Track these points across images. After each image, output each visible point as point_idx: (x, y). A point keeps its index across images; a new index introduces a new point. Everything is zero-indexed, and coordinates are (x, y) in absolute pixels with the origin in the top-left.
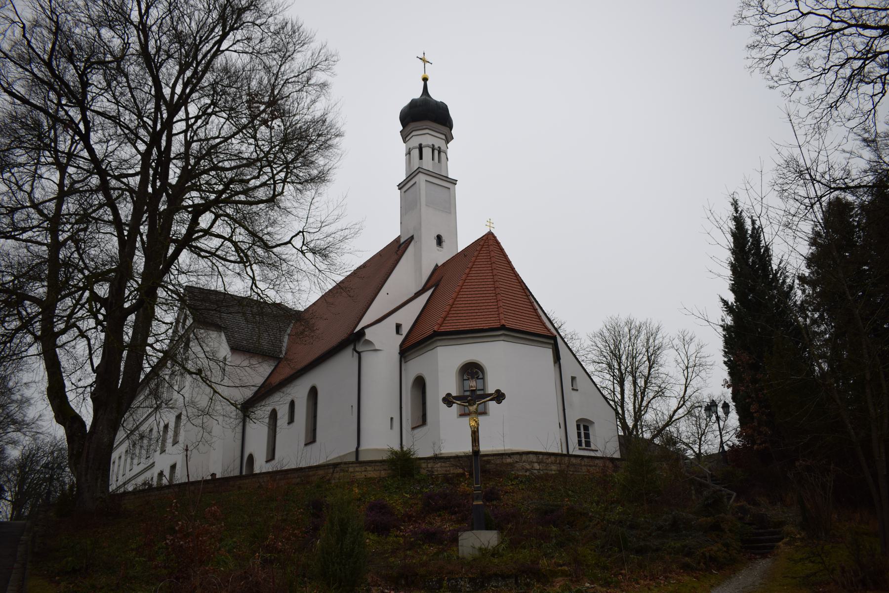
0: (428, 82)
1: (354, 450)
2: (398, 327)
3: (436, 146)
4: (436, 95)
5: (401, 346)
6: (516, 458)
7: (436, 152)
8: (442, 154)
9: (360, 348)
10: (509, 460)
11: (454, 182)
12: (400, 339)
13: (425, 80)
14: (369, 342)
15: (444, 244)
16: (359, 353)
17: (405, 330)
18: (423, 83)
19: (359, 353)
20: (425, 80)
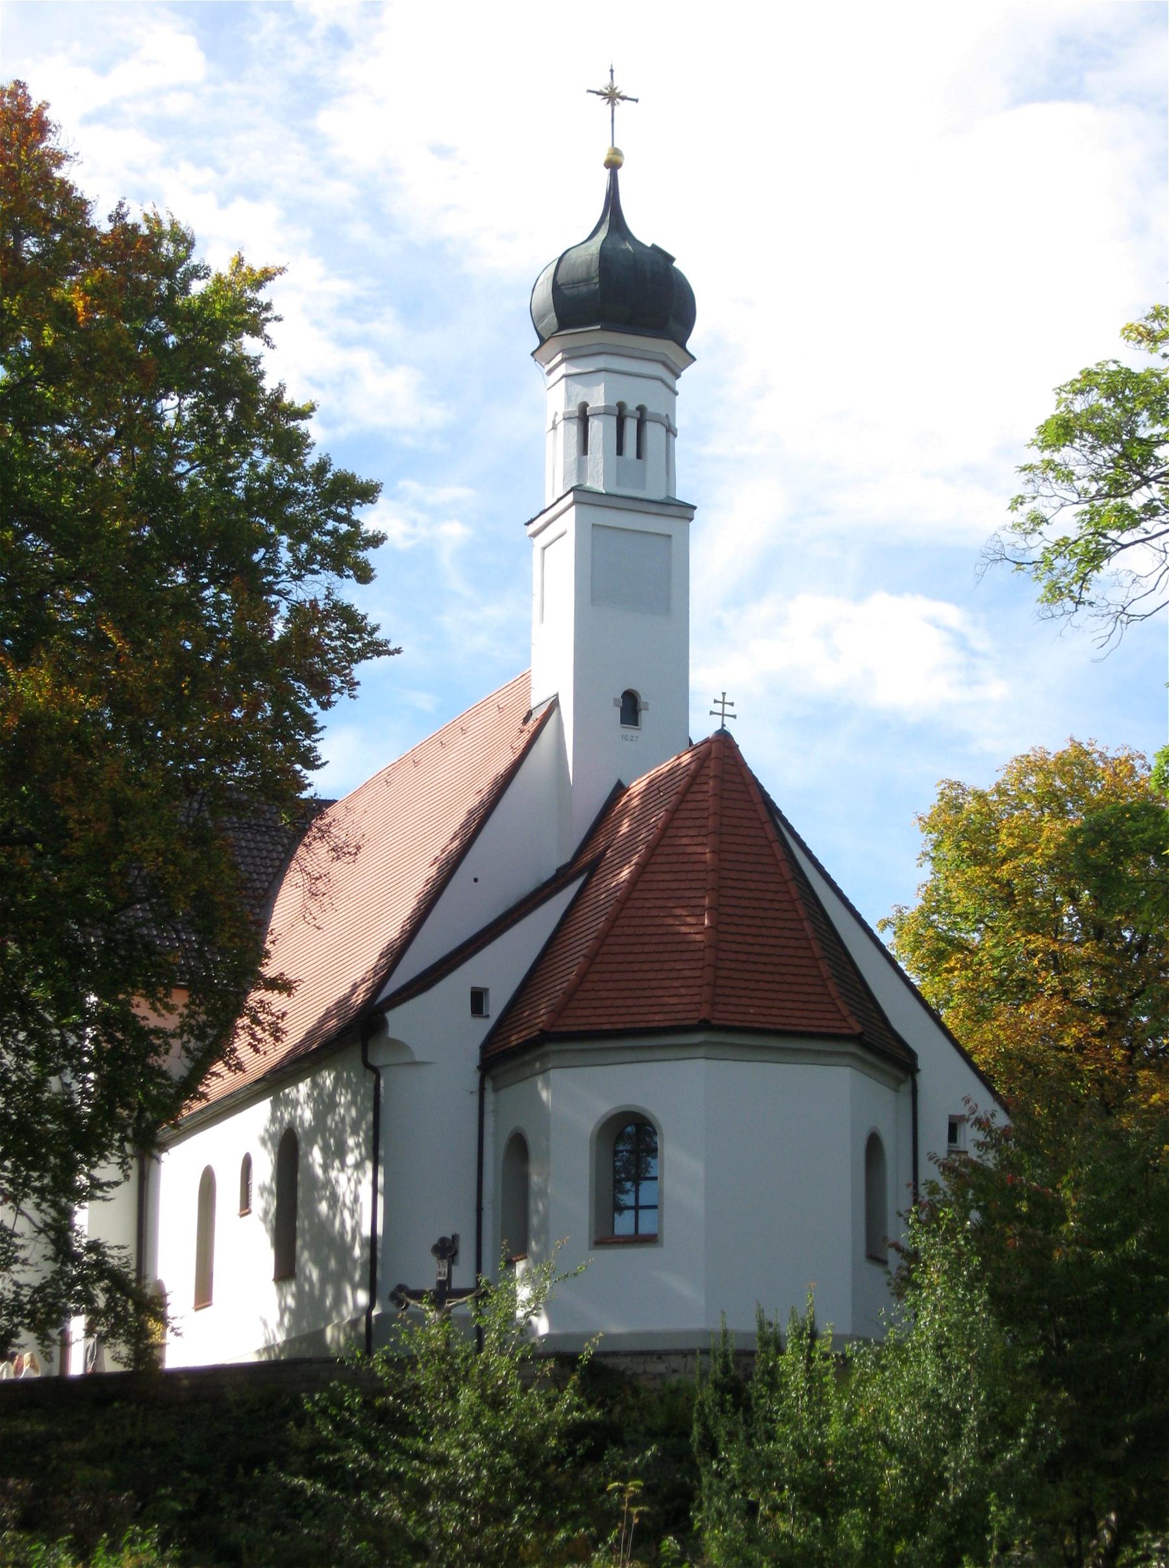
0: (619, 172)
1: (417, 1059)
2: (478, 999)
3: (631, 407)
4: (645, 228)
5: (484, 1048)
6: (675, 1362)
7: (631, 426)
8: (653, 432)
9: (377, 1059)
10: (661, 1367)
11: (685, 511)
12: (484, 1027)
13: (613, 165)
14: (398, 1045)
15: (644, 716)
16: (376, 1071)
17: (496, 1005)
18: (607, 172)
19: (376, 1071)
20: (613, 165)
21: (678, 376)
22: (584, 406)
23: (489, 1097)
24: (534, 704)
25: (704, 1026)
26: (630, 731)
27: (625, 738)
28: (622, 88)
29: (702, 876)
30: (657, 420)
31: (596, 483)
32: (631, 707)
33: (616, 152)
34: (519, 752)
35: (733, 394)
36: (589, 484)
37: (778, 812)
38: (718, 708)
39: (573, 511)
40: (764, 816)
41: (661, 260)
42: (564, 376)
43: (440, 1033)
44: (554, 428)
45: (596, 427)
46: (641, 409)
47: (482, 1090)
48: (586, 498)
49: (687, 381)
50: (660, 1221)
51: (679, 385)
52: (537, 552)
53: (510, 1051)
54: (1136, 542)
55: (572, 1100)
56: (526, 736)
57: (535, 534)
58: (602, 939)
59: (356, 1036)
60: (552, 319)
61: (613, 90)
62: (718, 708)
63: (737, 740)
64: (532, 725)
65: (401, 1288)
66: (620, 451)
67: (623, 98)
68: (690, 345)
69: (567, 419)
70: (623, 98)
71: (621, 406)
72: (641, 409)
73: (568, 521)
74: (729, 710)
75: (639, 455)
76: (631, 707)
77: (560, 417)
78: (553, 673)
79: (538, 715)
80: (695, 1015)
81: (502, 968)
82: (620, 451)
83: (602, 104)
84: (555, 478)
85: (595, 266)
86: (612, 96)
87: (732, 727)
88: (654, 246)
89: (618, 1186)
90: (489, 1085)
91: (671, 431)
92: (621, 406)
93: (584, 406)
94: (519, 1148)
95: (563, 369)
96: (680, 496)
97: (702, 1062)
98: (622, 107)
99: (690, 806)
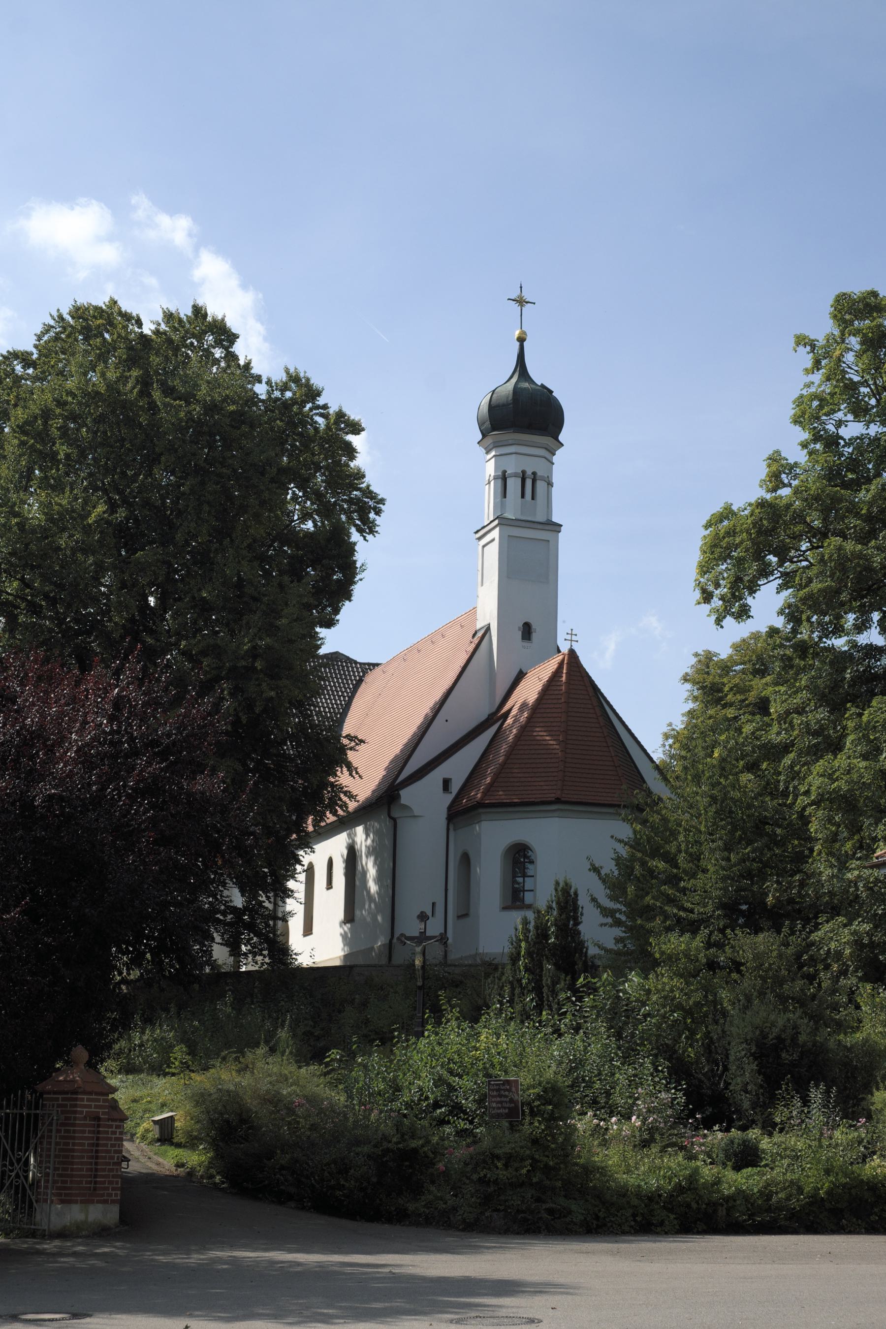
0: (525, 343)
2: (446, 784)
4: (539, 374)
5: (449, 808)
7: (529, 483)
8: (540, 485)
9: (395, 814)
12: (449, 798)
14: (406, 807)
17: (455, 788)
18: (518, 344)
20: (521, 340)
21: (554, 454)
22: (504, 472)
23: (451, 833)
24: (478, 627)
25: (558, 801)
26: (526, 644)
27: (524, 647)
28: (527, 296)
29: (560, 715)
30: (543, 479)
31: (509, 515)
32: (527, 631)
33: (524, 333)
34: (469, 654)
35: (575, 463)
36: (506, 515)
37: (599, 690)
38: (569, 637)
39: (497, 529)
40: (590, 689)
41: (547, 392)
42: (494, 456)
43: (427, 800)
44: (489, 483)
45: (510, 482)
46: (534, 474)
47: (448, 829)
48: (504, 522)
49: (559, 457)
50: (535, 897)
51: (555, 459)
52: (480, 548)
53: (461, 813)
54: (516, 453)
55: (494, 836)
56: (473, 646)
57: (480, 539)
58: (503, 765)
59: (386, 801)
60: (488, 424)
61: (522, 298)
62: (569, 637)
63: (578, 654)
64: (476, 640)
65: (402, 935)
66: (523, 496)
67: (527, 302)
68: (561, 438)
69: (495, 478)
70: (527, 302)
71: (524, 472)
72: (534, 474)
73: (495, 534)
74: (574, 638)
75: (533, 498)
76: (527, 631)
77: (492, 478)
78: (487, 611)
79: (480, 634)
80: (553, 795)
81: (458, 768)
82: (523, 496)
83: (516, 307)
84: (488, 512)
85: (511, 397)
86: (521, 302)
87: (576, 647)
88: (543, 386)
89: (514, 876)
90: (451, 827)
91: (550, 484)
92: (524, 472)
93: (504, 472)
94: (466, 860)
95: (493, 453)
96: (555, 519)
97: (557, 819)
98: (527, 308)
99: (553, 688)
